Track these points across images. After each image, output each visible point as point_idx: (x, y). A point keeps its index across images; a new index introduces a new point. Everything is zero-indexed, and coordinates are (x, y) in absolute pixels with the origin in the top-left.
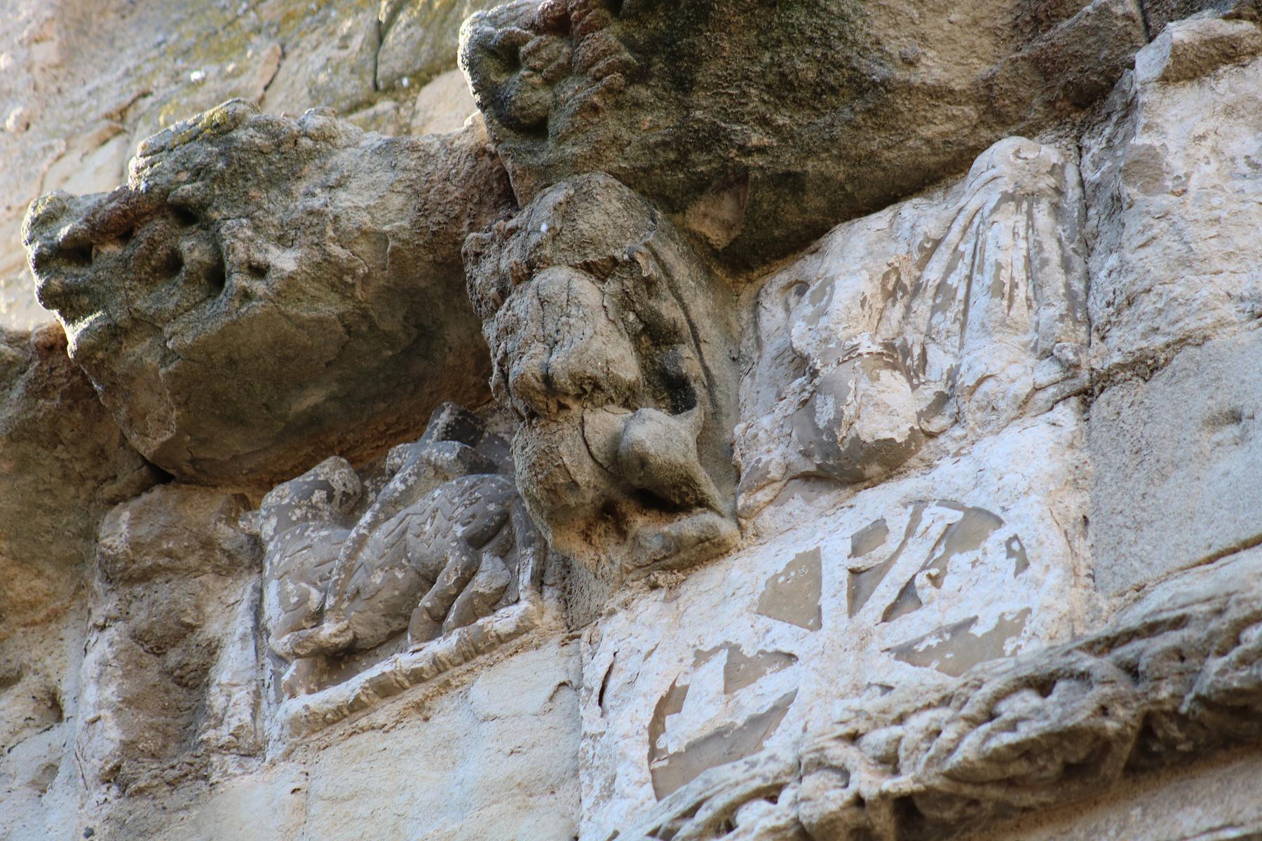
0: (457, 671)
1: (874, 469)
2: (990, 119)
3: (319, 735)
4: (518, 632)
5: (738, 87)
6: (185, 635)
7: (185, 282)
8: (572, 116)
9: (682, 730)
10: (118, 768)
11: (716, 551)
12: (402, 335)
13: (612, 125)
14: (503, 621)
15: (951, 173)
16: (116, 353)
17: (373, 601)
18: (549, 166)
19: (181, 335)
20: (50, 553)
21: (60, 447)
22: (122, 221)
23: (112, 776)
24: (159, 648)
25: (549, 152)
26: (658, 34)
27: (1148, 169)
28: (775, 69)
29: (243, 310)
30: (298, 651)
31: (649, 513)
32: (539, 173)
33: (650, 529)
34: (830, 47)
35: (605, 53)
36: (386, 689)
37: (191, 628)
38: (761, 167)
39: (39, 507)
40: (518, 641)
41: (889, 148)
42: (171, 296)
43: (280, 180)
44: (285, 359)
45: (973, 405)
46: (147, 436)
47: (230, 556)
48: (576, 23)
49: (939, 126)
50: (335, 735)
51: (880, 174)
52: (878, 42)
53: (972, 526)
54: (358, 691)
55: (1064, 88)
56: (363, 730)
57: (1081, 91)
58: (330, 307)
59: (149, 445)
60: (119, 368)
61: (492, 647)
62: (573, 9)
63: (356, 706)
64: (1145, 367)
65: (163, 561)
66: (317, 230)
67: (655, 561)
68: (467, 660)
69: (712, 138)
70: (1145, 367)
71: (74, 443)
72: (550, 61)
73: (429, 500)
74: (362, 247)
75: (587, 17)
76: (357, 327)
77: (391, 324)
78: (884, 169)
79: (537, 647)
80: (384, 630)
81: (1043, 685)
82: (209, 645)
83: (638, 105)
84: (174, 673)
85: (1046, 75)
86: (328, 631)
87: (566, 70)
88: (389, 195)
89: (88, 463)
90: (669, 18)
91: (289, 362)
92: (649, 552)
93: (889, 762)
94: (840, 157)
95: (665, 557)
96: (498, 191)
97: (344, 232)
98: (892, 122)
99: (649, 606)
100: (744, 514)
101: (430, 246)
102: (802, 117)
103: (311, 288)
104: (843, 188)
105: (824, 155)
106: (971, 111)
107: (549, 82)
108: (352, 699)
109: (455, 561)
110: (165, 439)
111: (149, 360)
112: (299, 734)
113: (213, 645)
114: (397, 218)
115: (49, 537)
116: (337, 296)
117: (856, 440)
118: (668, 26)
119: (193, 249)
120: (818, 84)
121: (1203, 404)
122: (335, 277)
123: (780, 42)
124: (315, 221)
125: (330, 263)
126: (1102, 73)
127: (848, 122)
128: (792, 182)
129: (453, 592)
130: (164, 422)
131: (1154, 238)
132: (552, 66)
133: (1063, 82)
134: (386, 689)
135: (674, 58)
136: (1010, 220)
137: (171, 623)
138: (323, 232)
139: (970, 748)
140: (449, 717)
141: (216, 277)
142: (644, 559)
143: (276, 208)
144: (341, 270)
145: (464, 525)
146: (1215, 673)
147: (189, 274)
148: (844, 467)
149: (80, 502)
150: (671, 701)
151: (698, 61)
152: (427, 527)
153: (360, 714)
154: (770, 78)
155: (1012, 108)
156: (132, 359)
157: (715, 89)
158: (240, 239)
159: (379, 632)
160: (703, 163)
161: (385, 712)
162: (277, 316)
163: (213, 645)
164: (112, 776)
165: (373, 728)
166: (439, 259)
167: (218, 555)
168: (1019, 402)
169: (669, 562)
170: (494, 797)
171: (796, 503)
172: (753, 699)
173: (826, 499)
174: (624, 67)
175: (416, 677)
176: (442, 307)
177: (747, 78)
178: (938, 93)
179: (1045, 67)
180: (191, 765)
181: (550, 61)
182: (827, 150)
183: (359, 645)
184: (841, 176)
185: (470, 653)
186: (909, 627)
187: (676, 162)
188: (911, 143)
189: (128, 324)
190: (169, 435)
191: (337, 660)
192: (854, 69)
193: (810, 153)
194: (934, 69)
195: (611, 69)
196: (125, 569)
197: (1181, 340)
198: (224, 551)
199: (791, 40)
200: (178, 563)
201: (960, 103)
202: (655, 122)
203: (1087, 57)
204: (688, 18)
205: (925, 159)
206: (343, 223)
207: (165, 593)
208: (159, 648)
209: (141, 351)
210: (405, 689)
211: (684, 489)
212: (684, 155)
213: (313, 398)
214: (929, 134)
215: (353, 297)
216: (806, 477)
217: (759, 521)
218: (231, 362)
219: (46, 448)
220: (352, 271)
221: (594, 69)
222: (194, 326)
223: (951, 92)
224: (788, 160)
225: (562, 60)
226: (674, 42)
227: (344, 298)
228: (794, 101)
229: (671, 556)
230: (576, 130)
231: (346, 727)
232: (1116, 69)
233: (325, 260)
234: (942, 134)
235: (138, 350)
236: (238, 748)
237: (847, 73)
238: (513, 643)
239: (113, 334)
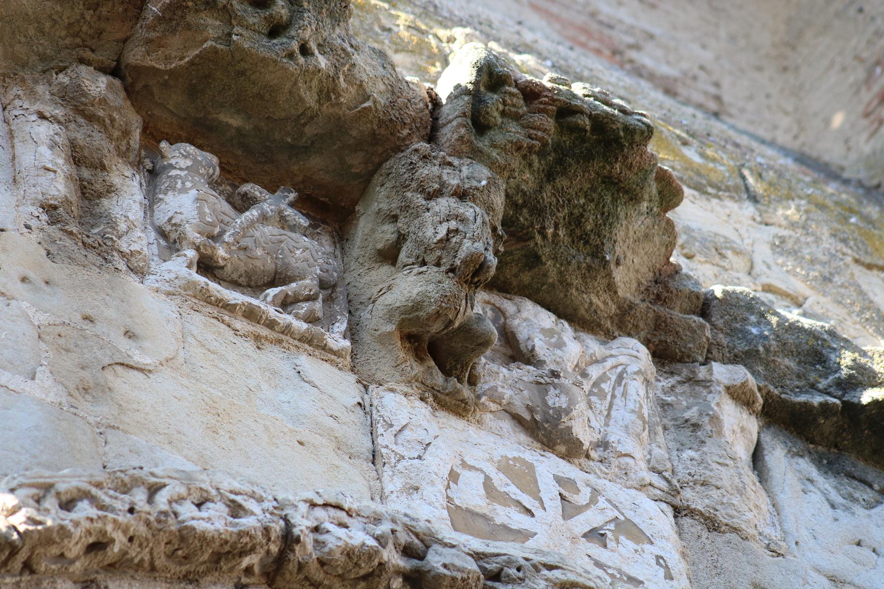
0: (291, 341)
1: (562, 449)
2: (616, 319)
3: (197, 301)
4: (334, 353)
5: (564, 201)
6: (96, 168)
7: (265, 18)
8: (508, 141)
10: (55, 208)
11: (460, 411)
12: (304, 139)
15: (579, 324)
16: (197, 11)
17: (250, 260)
18: (481, 152)
19: (243, 39)
20: (12, 46)
21: (91, 12)
23: (50, 209)
24: (79, 161)
26: (563, 144)
28: (581, 210)
29: (285, 61)
30: (201, 247)
32: (473, 149)
34: (605, 225)
35: (545, 130)
36: (251, 314)
37: (103, 168)
38: (537, 244)
39: (39, 22)
40: (333, 357)
41: (577, 289)
44: (260, 97)
45: (617, 463)
46: (149, 55)
47: (128, 149)
48: (541, 103)
49: (599, 302)
50: (207, 310)
51: (562, 295)
52: (615, 242)
54: (239, 302)
55: (660, 341)
56: (223, 321)
57: (666, 350)
58: (310, 99)
59: (135, 56)
60: (190, 18)
61: (318, 347)
62: (546, 96)
63: (230, 308)
64: (712, 524)
65: (108, 121)
66: (341, 60)
67: (433, 388)
68: (299, 340)
69: (538, 211)
71: (99, 18)
72: (514, 106)
73: (271, 226)
74: (353, 90)
75: (550, 107)
78: (566, 296)
79: (340, 369)
80: (235, 276)
82: (111, 186)
83: (530, 165)
85: (657, 327)
87: (517, 117)
88: (379, 79)
89: (91, 32)
90: (574, 143)
92: (434, 382)
94: (561, 272)
95: (439, 391)
97: (353, 75)
98: (589, 280)
100: (481, 407)
101: (381, 122)
102: (567, 240)
103: (315, 83)
104: (543, 285)
105: (558, 265)
106: (613, 308)
107: (503, 114)
108: (233, 302)
110: (157, 66)
111: (211, 31)
112: (185, 290)
113: (113, 189)
115: (23, 40)
116: (317, 97)
117: (569, 429)
118: (570, 147)
120: (586, 234)
122: (328, 91)
123: (593, 200)
124: (343, 55)
125: (334, 80)
126: (682, 352)
127: (579, 262)
129: (301, 298)
130: (166, 59)
131: (727, 465)
132: (513, 109)
133: (663, 338)
134: (251, 314)
135: (560, 161)
137: (95, 155)
138: (343, 65)
142: (428, 382)
144: (334, 89)
145: (321, 270)
147: (271, 16)
148: (546, 430)
149: (61, 43)
151: (564, 173)
152: (298, 252)
153: (226, 312)
154: (576, 211)
155: (630, 326)
156: (202, 22)
157: (559, 192)
159: (233, 275)
161: (241, 324)
162: (293, 79)
163: (113, 189)
164: (50, 209)
165: (229, 326)
166: (377, 132)
167: (124, 143)
168: (643, 483)
169: (439, 395)
170: (321, 432)
171: (507, 425)
173: (523, 437)
174: (545, 144)
175: (271, 324)
176: (335, 147)
177: (569, 201)
178: (611, 288)
180: (100, 245)
181: (514, 106)
182: (561, 265)
184: (551, 280)
187: (516, 205)
188: (585, 296)
189: (220, 5)
190: (162, 67)
192: (603, 244)
193: (555, 259)
195: (540, 139)
196: (86, 105)
197: (735, 529)
198: (128, 143)
199: (597, 205)
200: (110, 128)
201: (613, 300)
202: (528, 180)
203: (682, 339)
204: (582, 152)
205: (582, 309)
206: (356, 71)
208: (79, 161)
210: (258, 323)
211: (459, 366)
212: (524, 205)
214: (594, 301)
215: (321, 105)
216: (517, 419)
217: (484, 416)
218: (242, 73)
219: (84, 5)
220: (338, 96)
221: (532, 131)
223: (616, 292)
224: (545, 252)
225: (520, 111)
226: (566, 155)
227: (319, 101)
228: (571, 231)
229: (442, 393)
230: (504, 149)
231: (215, 311)
232: (689, 357)
233: (333, 78)
234: (597, 306)
235: (210, 21)
236: (128, 260)
237: (598, 242)
238: (329, 355)
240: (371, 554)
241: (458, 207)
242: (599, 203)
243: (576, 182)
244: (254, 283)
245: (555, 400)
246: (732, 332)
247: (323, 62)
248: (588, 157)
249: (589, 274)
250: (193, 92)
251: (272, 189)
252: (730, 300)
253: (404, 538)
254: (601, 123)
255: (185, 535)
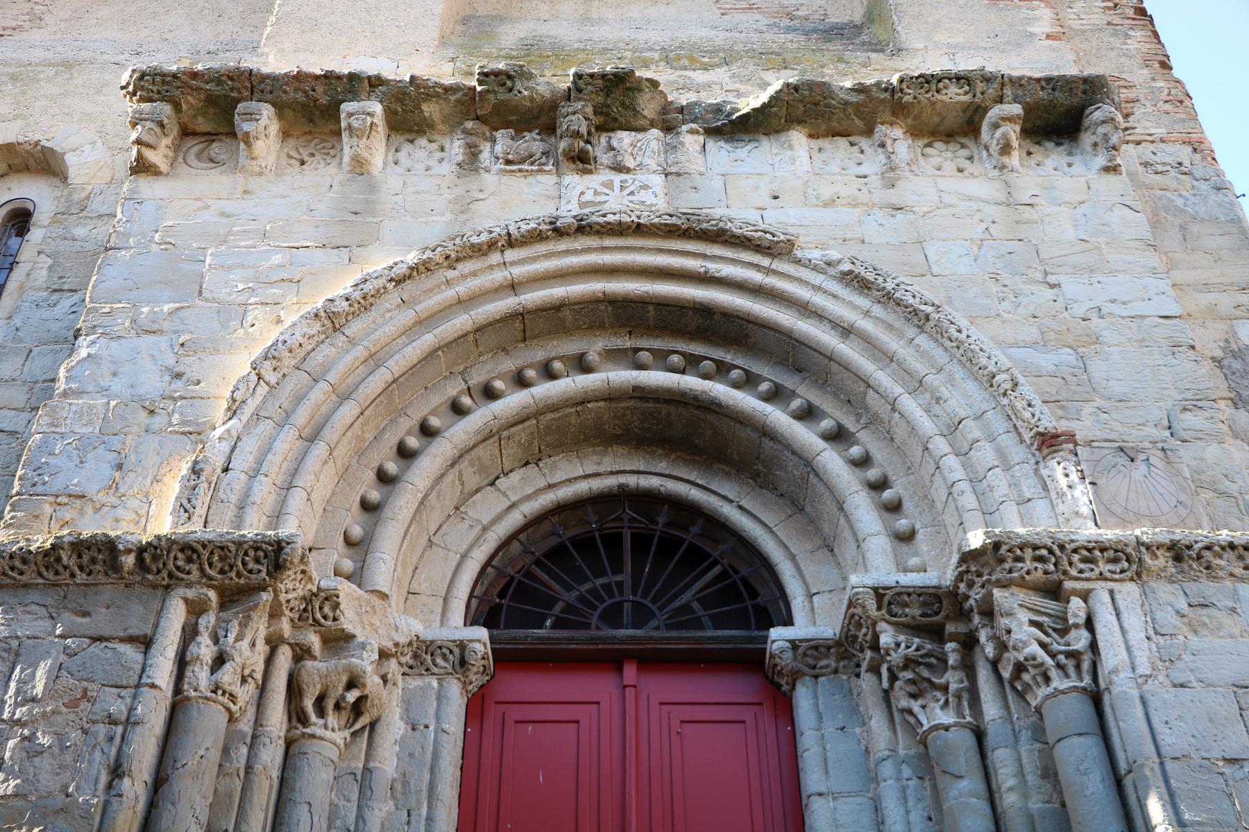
9: (584, 199)
13: (594, 96)
14: (546, 168)
22: (497, 74)
23: (459, 164)
25: (581, 96)
27: (682, 143)
31: (582, 160)
33: (581, 165)
36: (520, 170)
42: (502, 89)
43: (528, 79)
49: (642, 122)
53: (645, 187)
58: (528, 104)
59: (479, 113)
64: (678, 174)
69: (608, 106)
70: (678, 174)
73: (533, 143)
76: (530, 109)
77: (247, 127)
81: (671, 216)
84: (473, 154)
86: (510, 157)
91: (515, 109)
93: (639, 217)
96: (568, 96)
99: (577, 177)
109: (538, 155)
114: (547, 95)
119: (509, 83)
121: (1032, 150)
122: (532, 99)
128: (615, 120)
134: (520, 170)
136: (655, 142)
139: (656, 220)
140: (530, 179)
141: (510, 90)
143: (526, 83)
146: (705, 225)
148: (619, 168)
150: (582, 193)
158: (518, 85)
160: (604, 110)
164: (459, 164)
171: (607, 170)
172: (599, 199)
178: (645, 117)
179: (664, 121)
183: (944, 138)
185: (539, 171)
186: (631, 198)
191: (508, 162)
194: (645, 113)
202: (600, 99)
207: (474, 139)
209: (491, 96)
213: (514, 118)
222: (503, 96)
239: (488, 91)
240: (535, 229)
241: (577, 118)
242: (628, 97)
243: (617, 93)
244: (522, 161)
245: (619, 158)
246: (690, 114)
247: (526, 93)
248: (617, 86)
249: (635, 116)
250: (498, 115)
251: (530, 131)
252: (689, 105)
253: (547, 220)
254: (615, 75)
255: (473, 245)
